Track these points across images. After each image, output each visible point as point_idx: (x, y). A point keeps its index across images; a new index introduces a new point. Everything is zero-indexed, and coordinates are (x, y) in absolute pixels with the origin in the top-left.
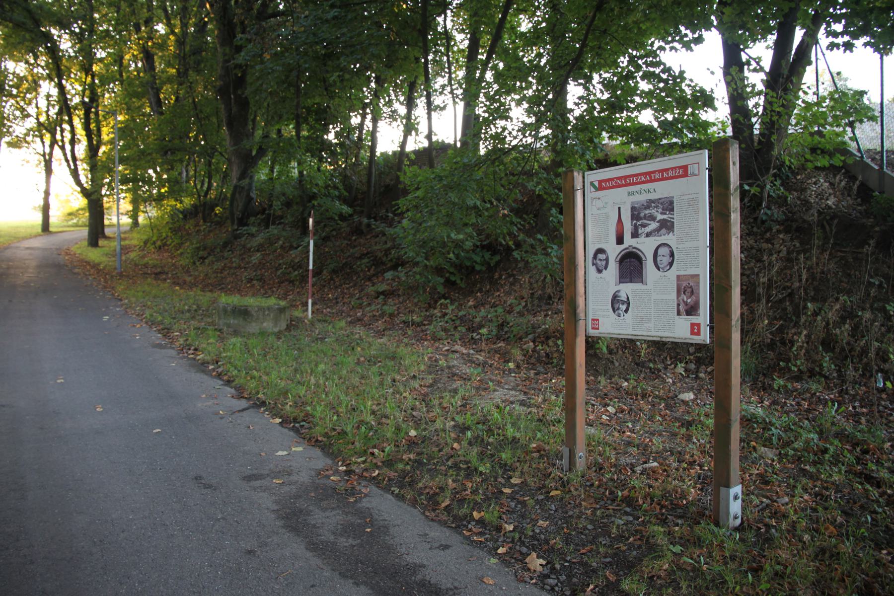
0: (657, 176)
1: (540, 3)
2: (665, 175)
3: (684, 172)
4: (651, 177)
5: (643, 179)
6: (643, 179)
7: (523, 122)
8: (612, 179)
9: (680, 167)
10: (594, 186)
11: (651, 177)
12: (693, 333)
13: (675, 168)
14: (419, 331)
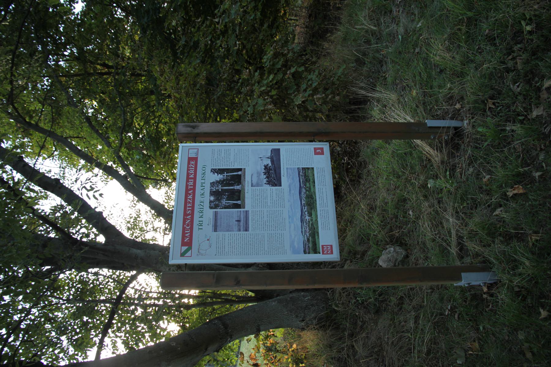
0: (191, 184)
1: (2, 313)
3: (193, 161)
4: (191, 189)
5: (190, 197)
6: (190, 197)
7: (39, 204)
8: (184, 229)
9: (189, 163)
10: (186, 251)
12: (322, 153)
13: (188, 167)
14: (244, 195)
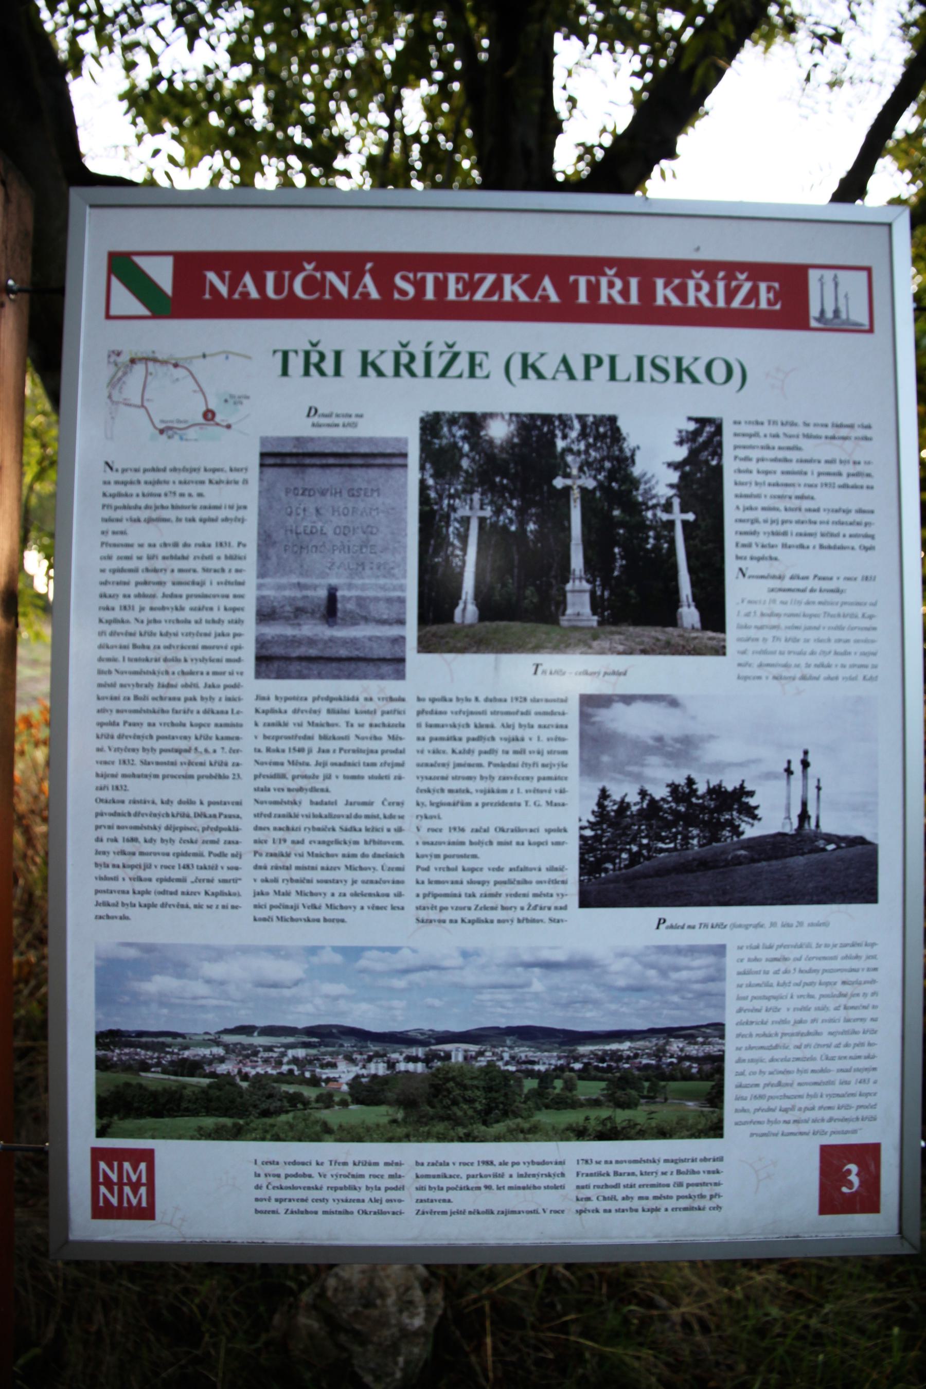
2: (663, 293)
6: (511, 289)
9: (759, 271)
11: (567, 291)
12: (832, 1201)
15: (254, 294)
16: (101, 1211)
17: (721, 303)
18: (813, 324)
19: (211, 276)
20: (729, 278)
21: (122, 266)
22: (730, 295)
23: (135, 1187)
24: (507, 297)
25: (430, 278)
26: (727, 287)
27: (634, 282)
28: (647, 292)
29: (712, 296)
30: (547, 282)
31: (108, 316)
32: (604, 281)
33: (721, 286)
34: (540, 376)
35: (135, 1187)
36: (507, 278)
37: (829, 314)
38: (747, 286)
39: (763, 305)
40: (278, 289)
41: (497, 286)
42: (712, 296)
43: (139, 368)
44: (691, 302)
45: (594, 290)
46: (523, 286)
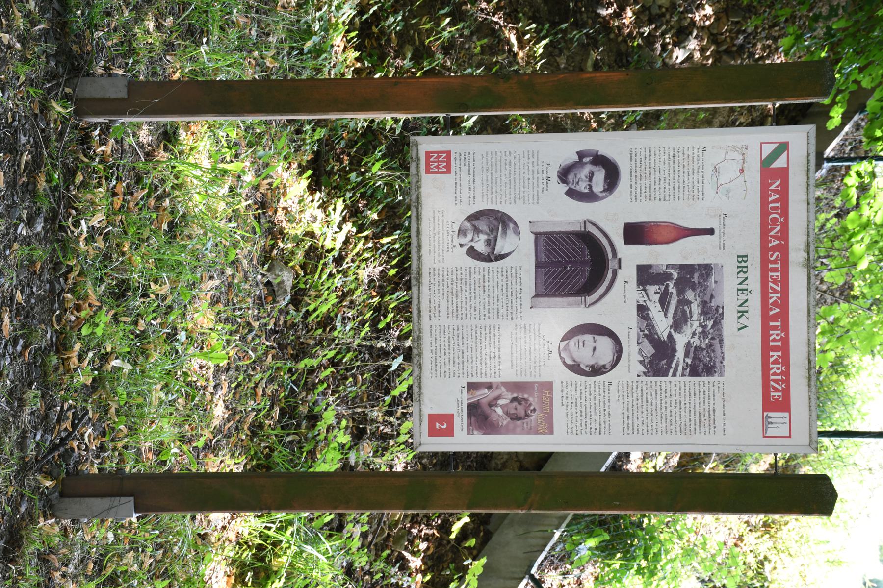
2: (775, 355)
6: (774, 297)
9: (787, 392)
11: (775, 318)
12: (433, 418)
13: (787, 381)
15: (770, 199)
16: (428, 154)
17: (772, 377)
18: (765, 414)
19: (778, 182)
20: (783, 381)
21: (783, 147)
22: (775, 381)
23: (437, 167)
24: (771, 295)
25: (778, 266)
26: (779, 380)
27: (779, 344)
28: (776, 348)
29: (775, 374)
30: (778, 310)
31: (761, 143)
32: (779, 332)
33: (780, 377)
34: (739, 318)
35: (437, 167)
36: (779, 295)
37: (770, 420)
38: (780, 388)
39: (772, 394)
40: (772, 208)
41: (775, 291)
42: (775, 374)
43: (741, 157)
44: (772, 366)
45: (775, 328)
46: (776, 301)
